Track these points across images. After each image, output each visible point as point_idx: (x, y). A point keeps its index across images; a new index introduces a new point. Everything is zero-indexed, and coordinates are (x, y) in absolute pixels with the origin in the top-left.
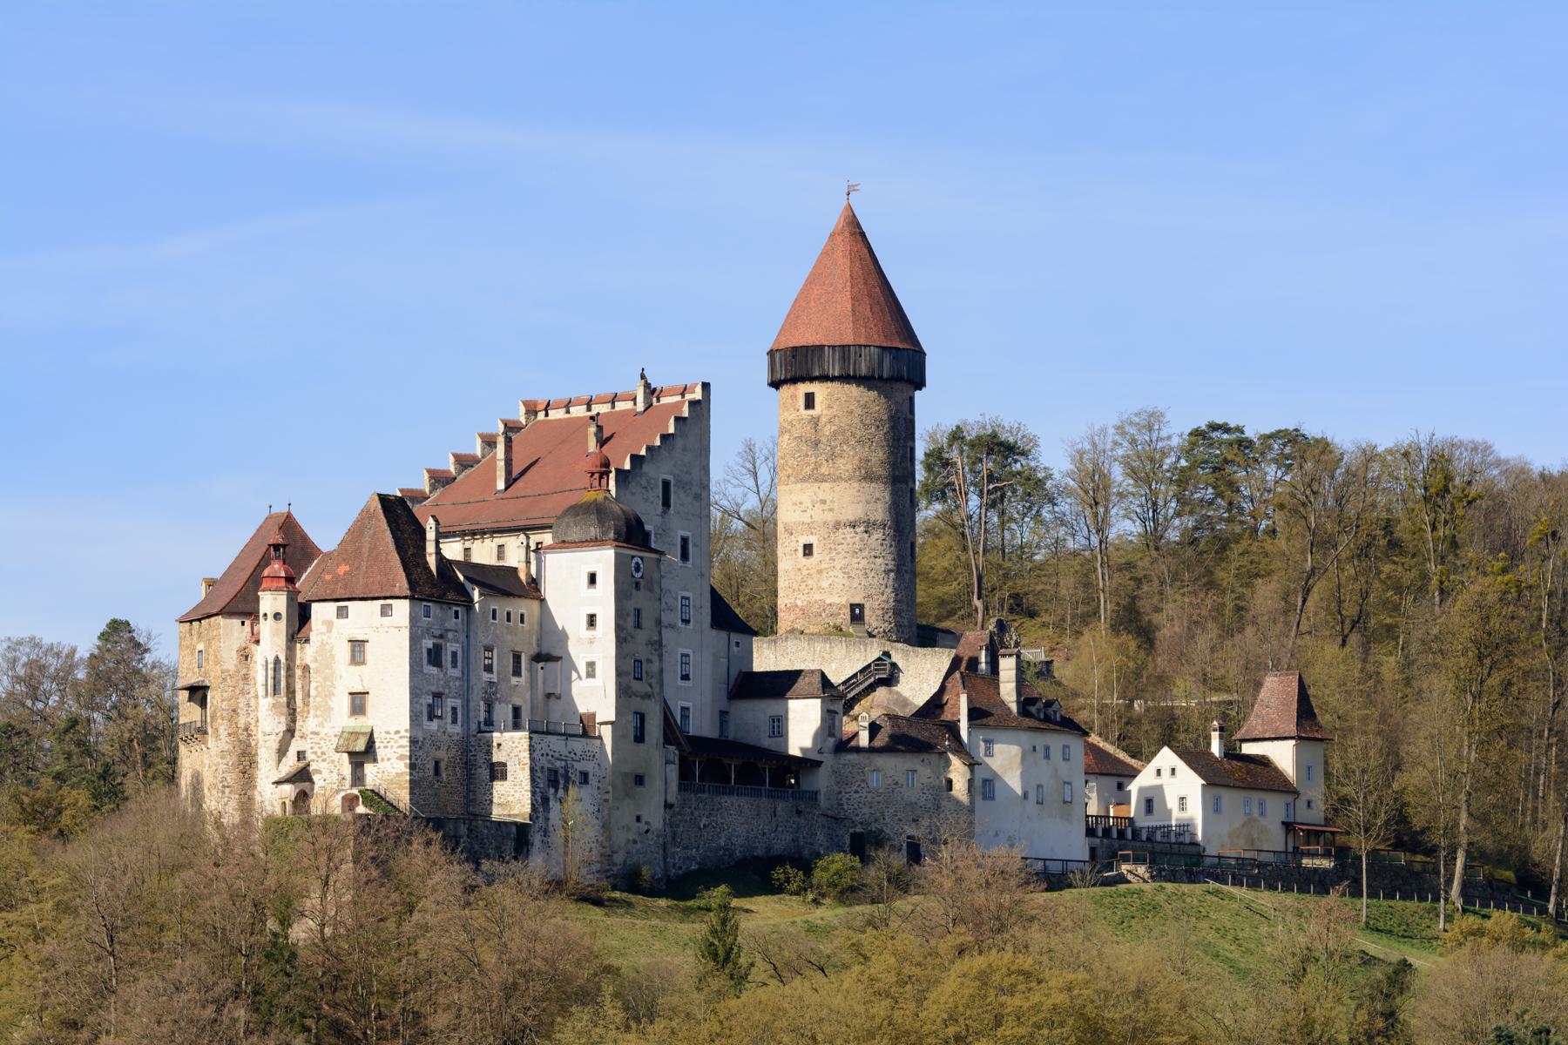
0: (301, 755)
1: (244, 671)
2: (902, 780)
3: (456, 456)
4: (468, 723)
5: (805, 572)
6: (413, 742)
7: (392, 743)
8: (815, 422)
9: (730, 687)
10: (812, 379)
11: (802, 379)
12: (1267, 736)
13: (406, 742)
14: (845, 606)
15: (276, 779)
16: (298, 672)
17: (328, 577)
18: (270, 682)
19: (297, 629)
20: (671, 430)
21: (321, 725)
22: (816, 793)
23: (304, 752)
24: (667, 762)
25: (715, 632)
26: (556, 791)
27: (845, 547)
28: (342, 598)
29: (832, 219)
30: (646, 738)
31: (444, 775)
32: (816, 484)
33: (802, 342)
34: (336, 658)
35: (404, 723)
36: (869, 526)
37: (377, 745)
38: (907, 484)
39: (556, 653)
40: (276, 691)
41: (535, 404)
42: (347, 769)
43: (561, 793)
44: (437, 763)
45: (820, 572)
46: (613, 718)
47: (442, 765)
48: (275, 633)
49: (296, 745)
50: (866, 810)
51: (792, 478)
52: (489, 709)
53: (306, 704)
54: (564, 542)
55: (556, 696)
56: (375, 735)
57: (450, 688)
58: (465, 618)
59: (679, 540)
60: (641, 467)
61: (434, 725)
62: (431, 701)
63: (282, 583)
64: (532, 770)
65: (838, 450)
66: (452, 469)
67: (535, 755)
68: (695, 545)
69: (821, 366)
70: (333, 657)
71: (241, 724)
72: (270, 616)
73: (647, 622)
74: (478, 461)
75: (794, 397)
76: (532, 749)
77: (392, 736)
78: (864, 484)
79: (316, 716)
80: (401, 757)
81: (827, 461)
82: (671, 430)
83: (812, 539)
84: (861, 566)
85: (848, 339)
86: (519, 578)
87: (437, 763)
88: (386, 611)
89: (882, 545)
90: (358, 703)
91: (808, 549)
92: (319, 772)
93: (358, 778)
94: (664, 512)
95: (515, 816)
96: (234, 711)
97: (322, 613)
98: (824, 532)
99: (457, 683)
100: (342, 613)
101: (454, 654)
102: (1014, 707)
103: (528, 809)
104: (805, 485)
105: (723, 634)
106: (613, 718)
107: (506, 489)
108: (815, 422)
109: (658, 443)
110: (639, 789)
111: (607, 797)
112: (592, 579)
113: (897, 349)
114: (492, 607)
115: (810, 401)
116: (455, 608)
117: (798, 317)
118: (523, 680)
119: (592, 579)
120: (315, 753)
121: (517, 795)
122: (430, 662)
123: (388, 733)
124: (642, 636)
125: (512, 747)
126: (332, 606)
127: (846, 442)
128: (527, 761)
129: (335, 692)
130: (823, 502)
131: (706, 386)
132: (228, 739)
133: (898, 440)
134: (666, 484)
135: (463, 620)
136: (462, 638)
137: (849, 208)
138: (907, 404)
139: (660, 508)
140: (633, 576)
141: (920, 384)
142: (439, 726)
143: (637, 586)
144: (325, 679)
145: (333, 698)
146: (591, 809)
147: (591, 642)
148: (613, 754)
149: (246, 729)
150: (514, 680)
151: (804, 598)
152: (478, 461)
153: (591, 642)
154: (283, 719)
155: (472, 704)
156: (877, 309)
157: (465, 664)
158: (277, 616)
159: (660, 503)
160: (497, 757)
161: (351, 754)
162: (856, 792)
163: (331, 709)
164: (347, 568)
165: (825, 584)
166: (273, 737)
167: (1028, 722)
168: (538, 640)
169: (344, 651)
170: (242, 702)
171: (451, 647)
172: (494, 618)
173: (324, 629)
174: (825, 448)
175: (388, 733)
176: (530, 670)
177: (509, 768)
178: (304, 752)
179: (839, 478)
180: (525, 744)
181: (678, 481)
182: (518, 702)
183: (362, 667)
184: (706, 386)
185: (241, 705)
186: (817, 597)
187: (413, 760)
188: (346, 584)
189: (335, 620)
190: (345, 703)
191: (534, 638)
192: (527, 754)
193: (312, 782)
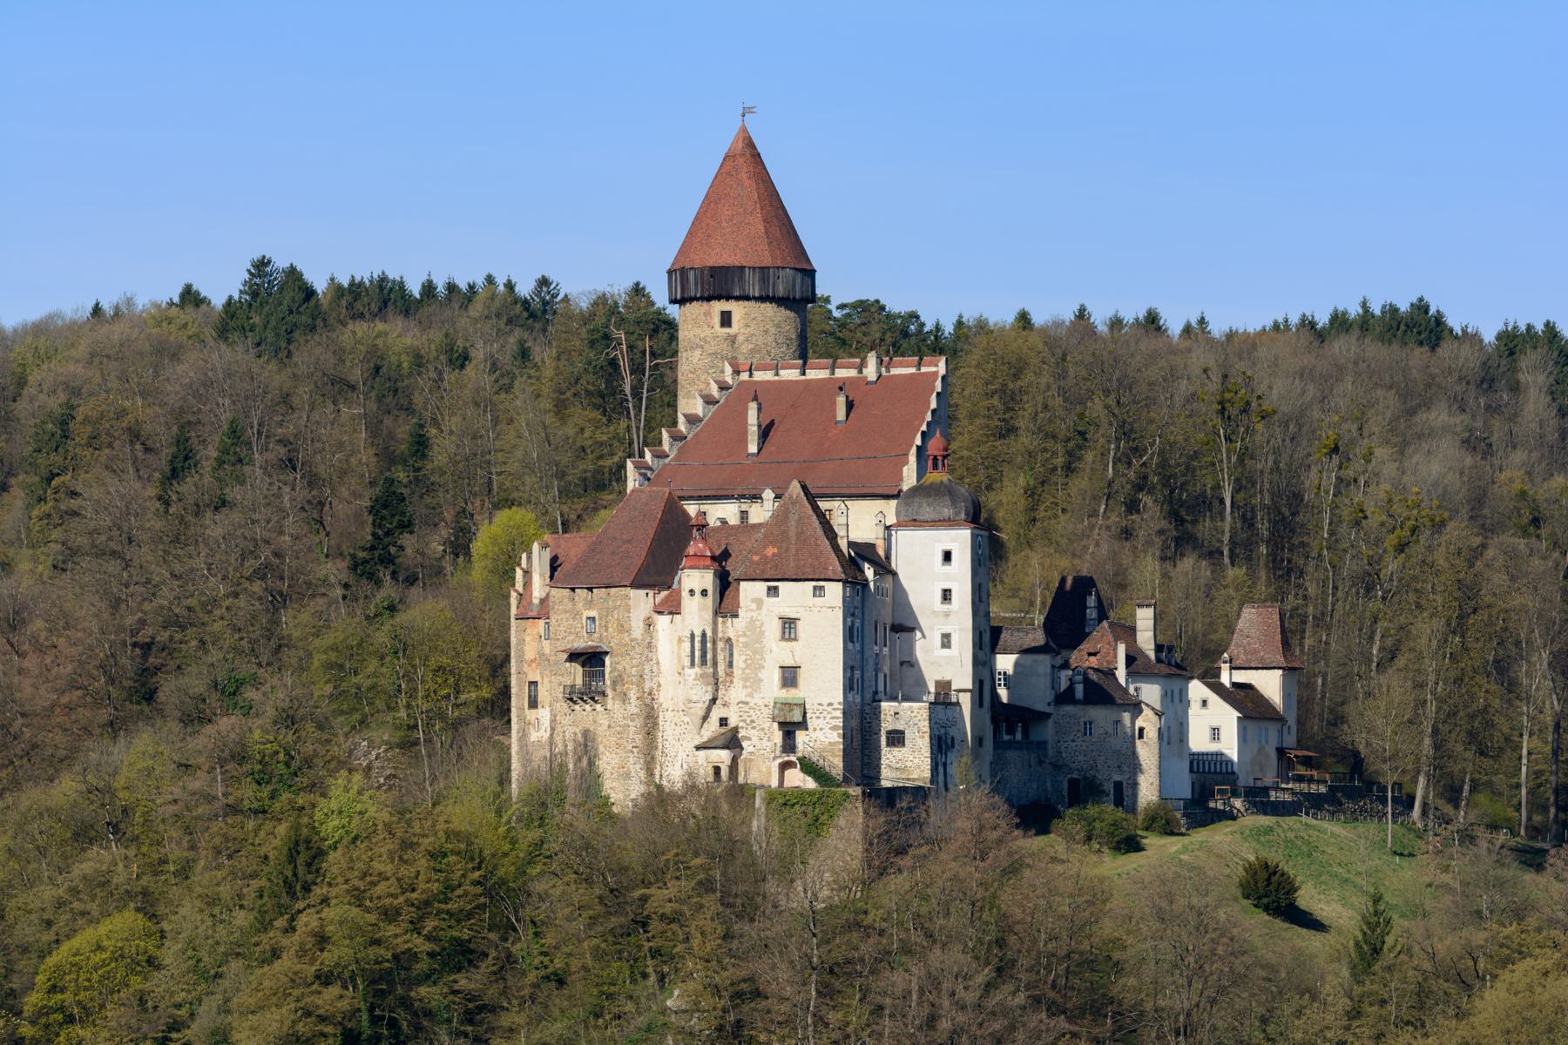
0: (723, 722)
2: (1111, 731)
7: (825, 713)
8: (732, 340)
10: (728, 298)
11: (719, 298)
12: (1253, 665)
13: (839, 714)
15: (697, 743)
16: (720, 645)
17: (756, 558)
18: (697, 654)
21: (751, 695)
22: (1045, 743)
23: (726, 719)
28: (774, 577)
29: (723, 142)
33: (721, 263)
34: (766, 634)
35: (836, 694)
39: (910, 625)
40: (704, 662)
42: (778, 736)
48: (702, 608)
49: (717, 714)
50: (1081, 758)
53: (730, 674)
54: (915, 520)
63: (708, 562)
69: (742, 287)
70: (762, 633)
74: (701, 420)
75: (708, 314)
80: (834, 728)
85: (767, 261)
88: (819, 592)
90: (790, 676)
92: (749, 739)
93: (789, 745)
95: (914, 780)
100: (773, 592)
102: (1152, 655)
103: (927, 774)
107: (759, 451)
108: (732, 340)
112: (947, 556)
115: (726, 319)
117: (709, 236)
119: (947, 556)
120: (744, 721)
123: (821, 705)
126: (763, 586)
137: (744, 130)
144: (755, 653)
147: (947, 615)
149: (650, 694)
152: (701, 420)
153: (947, 615)
154: (710, 688)
155: (867, 675)
158: (704, 593)
161: (782, 724)
162: (1073, 741)
163: (760, 681)
164: (776, 550)
166: (700, 705)
167: (1164, 668)
169: (773, 628)
170: (647, 668)
173: (754, 606)
175: (821, 705)
177: (907, 735)
178: (726, 719)
180: (925, 714)
183: (794, 643)
188: (776, 566)
189: (765, 599)
190: (776, 676)
193: (742, 749)
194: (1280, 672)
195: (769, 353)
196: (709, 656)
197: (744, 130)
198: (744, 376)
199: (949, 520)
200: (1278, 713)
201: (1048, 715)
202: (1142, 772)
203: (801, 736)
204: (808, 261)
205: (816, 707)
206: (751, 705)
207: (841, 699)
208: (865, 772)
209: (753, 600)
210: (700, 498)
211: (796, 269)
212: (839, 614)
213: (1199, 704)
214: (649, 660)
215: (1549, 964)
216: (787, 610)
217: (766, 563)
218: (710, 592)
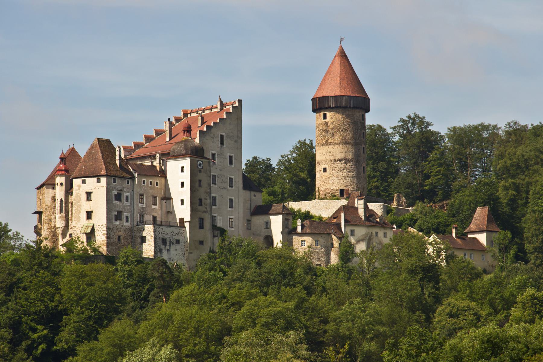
1: (54, 205)
3: (156, 130)
4: (133, 221)
5: (324, 178)
6: (108, 228)
8: (327, 123)
9: (252, 211)
13: (105, 229)
14: (338, 190)
16: (70, 205)
19: (69, 188)
20: (225, 117)
24: (214, 236)
25: (244, 191)
26: (165, 247)
27: (338, 168)
28: (84, 176)
29: (335, 51)
30: (204, 227)
31: (122, 241)
32: (328, 146)
35: (104, 221)
36: (346, 161)
37: (95, 230)
38: (361, 145)
41: (187, 111)
43: (168, 247)
44: (119, 237)
45: (329, 178)
46: (190, 220)
47: (122, 238)
48: (61, 191)
49: (70, 232)
51: (319, 144)
52: (142, 216)
55: (171, 212)
56: (95, 227)
57: (125, 209)
58: (132, 183)
59: (228, 157)
60: (211, 130)
61: (118, 223)
62: (116, 214)
64: (155, 238)
65: (335, 134)
66: (154, 135)
67: (156, 233)
68: (235, 159)
70: (80, 198)
71: (53, 225)
72: (59, 184)
73: (204, 184)
75: (320, 115)
76: (155, 231)
77: (101, 227)
78: (344, 146)
79: (75, 220)
80: (104, 235)
81: (331, 137)
82: (225, 117)
83: (326, 166)
84: (343, 175)
85: (338, 94)
86: (157, 169)
87: (119, 237)
88: (99, 181)
89: (351, 167)
90: (89, 215)
91: (325, 170)
94: (221, 147)
96: (50, 220)
97: (77, 182)
98: (330, 163)
99: (129, 208)
101: (127, 197)
102: (363, 218)
104: (324, 146)
105: (248, 193)
106: (190, 220)
108: (327, 123)
109: (218, 121)
110: (201, 246)
111: (187, 249)
113: (356, 97)
114: (143, 179)
116: (127, 180)
118: (157, 207)
121: (150, 248)
122: (116, 200)
123: (99, 226)
125: (149, 231)
127: (338, 131)
128: (153, 235)
129: (81, 211)
130: (330, 152)
131: (240, 101)
132: (47, 230)
133: (358, 129)
134: (222, 137)
135: (131, 184)
136: (131, 191)
138: (361, 118)
139: (220, 145)
140: (198, 168)
141: (368, 110)
142: (120, 223)
143: (200, 171)
145: (81, 214)
146: (181, 253)
148: (190, 233)
150: (153, 207)
151: (324, 187)
154: (64, 222)
155: (135, 215)
156: (349, 82)
157: (132, 201)
159: (220, 143)
160: (144, 234)
165: (331, 182)
166: (60, 229)
167: (367, 223)
168: (164, 192)
169: (84, 196)
171: (125, 194)
172: (144, 183)
173: (77, 188)
174: (330, 133)
175: (99, 226)
176: (161, 203)
179: (335, 144)
181: (228, 136)
182: (155, 214)
184: (240, 101)
185: (53, 218)
186: (328, 187)
187: (108, 235)
190: (85, 215)
191: (163, 191)
192: (153, 233)
202: (146, 242)
206: (77, 227)
207: (106, 223)
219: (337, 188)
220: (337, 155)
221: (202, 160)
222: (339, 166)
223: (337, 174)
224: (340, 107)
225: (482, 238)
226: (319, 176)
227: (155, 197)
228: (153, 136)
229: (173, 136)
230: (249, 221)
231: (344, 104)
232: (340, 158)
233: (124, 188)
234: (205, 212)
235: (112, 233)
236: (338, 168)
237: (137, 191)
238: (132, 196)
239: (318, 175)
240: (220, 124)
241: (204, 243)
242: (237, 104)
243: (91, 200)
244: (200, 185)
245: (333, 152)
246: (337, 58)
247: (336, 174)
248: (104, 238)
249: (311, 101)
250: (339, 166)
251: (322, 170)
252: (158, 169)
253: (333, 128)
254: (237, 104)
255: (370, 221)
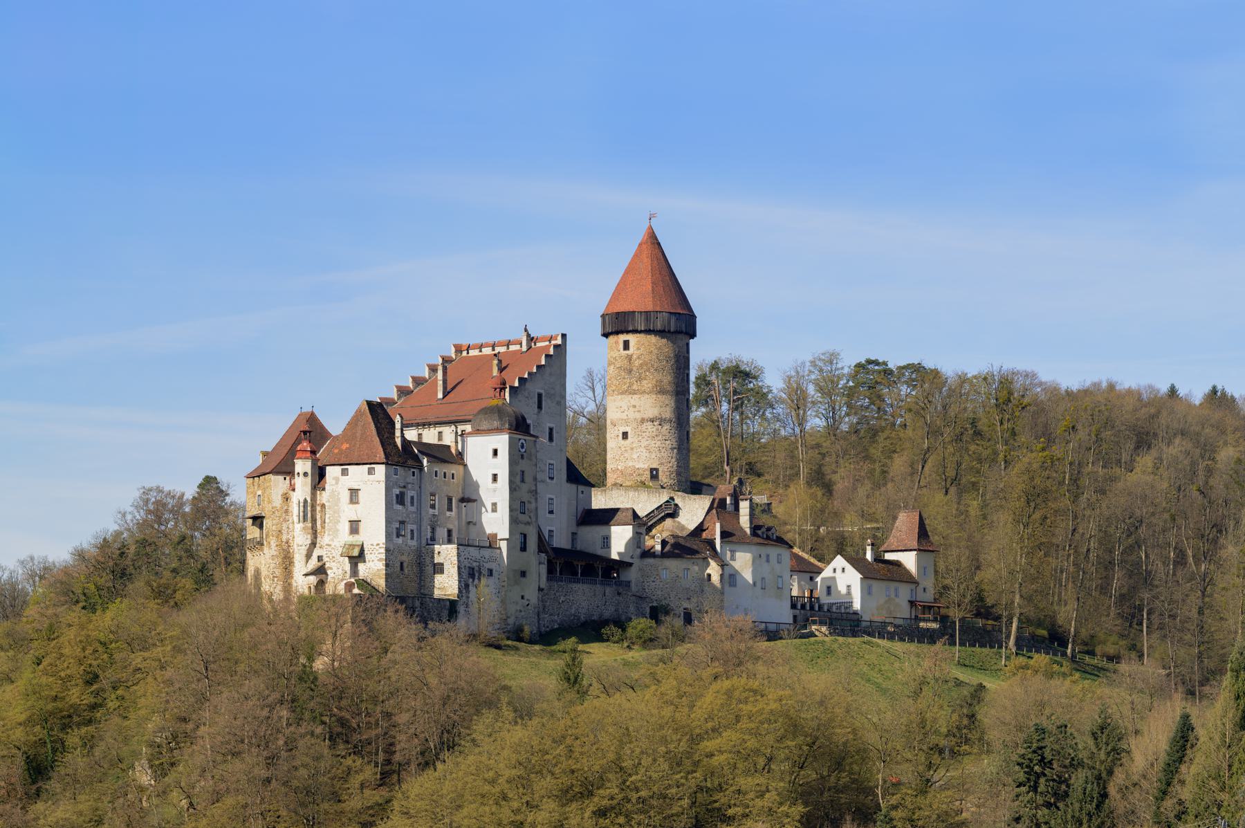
0: (320, 558)
6: (387, 550)
8: (630, 358)
10: (628, 332)
11: (622, 332)
12: (900, 549)
13: (383, 551)
16: (318, 508)
17: (336, 451)
18: (301, 514)
20: (543, 363)
21: (332, 540)
26: (473, 581)
27: (647, 433)
28: (345, 463)
29: (640, 235)
31: (406, 571)
32: (630, 396)
33: (622, 309)
35: (382, 539)
36: (662, 421)
37: (366, 552)
39: (474, 498)
40: (305, 519)
42: (347, 567)
43: (476, 581)
45: (632, 449)
46: (508, 537)
47: (405, 565)
51: (616, 392)
53: (323, 527)
56: (365, 546)
61: (400, 540)
64: (459, 568)
65: (643, 375)
66: (411, 386)
69: (633, 325)
70: (339, 499)
71: (284, 540)
72: (301, 475)
73: (528, 478)
75: (617, 343)
76: (459, 555)
79: (329, 535)
80: (380, 560)
82: (543, 363)
85: (650, 308)
88: (371, 472)
90: (354, 527)
91: (625, 435)
92: (331, 568)
97: (332, 472)
98: (635, 425)
100: (345, 472)
101: (412, 498)
102: (748, 531)
103: (456, 591)
105: (574, 486)
106: (508, 537)
108: (630, 358)
110: (523, 579)
111: (503, 584)
112: (495, 452)
113: (679, 314)
115: (626, 345)
116: (413, 470)
118: (453, 514)
119: (495, 452)
122: (397, 503)
123: (372, 545)
124: (525, 487)
125: (447, 554)
127: (648, 370)
128: (456, 562)
130: (634, 406)
131: (564, 336)
134: (540, 396)
137: (651, 228)
139: (536, 410)
141: (693, 335)
146: (494, 591)
149: (287, 543)
150: (448, 514)
154: (309, 536)
155: (423, 528)
158: (305, 474)
162: (653, 582)
163: (338, 530)
164: (348, 446)
165: (635, 456)
166: (304, 547)
169: (346, 495)
170: (285, 526)
173: (334, 482)
175: (372, 545)
176: (458, 507)
179: (644, 392)
180: (455, 552)
182: (451, 527)
183: (357, 505)
186: (631, 464)
189: (340, 477)
190: (347, 526)
191: (460, 488)
192: (456, 558)
193: (327, 574)
194: (915, 552)
195: (652, 366)
196: (309, 515)
197: (651, 228)
198: (464, 353)
199: (498, 429)
200: (911, 575)
201: (630, 565)
203: (361, 566)
204: (693, 312)
205: (370, 546)
207: (384, 541)
208: (422, 591)
209: (334, 479)
210: (417, 425)
211: (670, 313)
212: (383, 485)
213: (841, 570)
214: (286, 520)
215: (1047, 742)
216: (353, 483)
217: (342, 454)
218: (310, 474)
219: (646, 466)
220: (646, 412)
221: (525, 438)
222: (650, 430)
223: (647, 442)
224: (653, 331)
225: (909, 560)
226: (614, 446)
227: (450, 500)
228: (409, 387)
229: (448, 389)
230: (574, 534)
231: (659, 327)
232: (651, 417)
233: (408, 483)
234: (528, 523)
235: (392, 557)
236: (647, 433)
237: (428, 488)
238: (420, 495)
239: (611, 444)
240: (538, 375)
241: (527, 574)
242: (559, 341)
243: (357, 503)
244: (523, 481)
245: (640, 406)
246: (644, 246)
247: (644, 443)
248: (381, 566)
249: (600, 320)
250: (650, 430)
251: (621, 435)
252: (453, 451)
253: (641, 365)
254: (559, 341)
255: (757, 536)
